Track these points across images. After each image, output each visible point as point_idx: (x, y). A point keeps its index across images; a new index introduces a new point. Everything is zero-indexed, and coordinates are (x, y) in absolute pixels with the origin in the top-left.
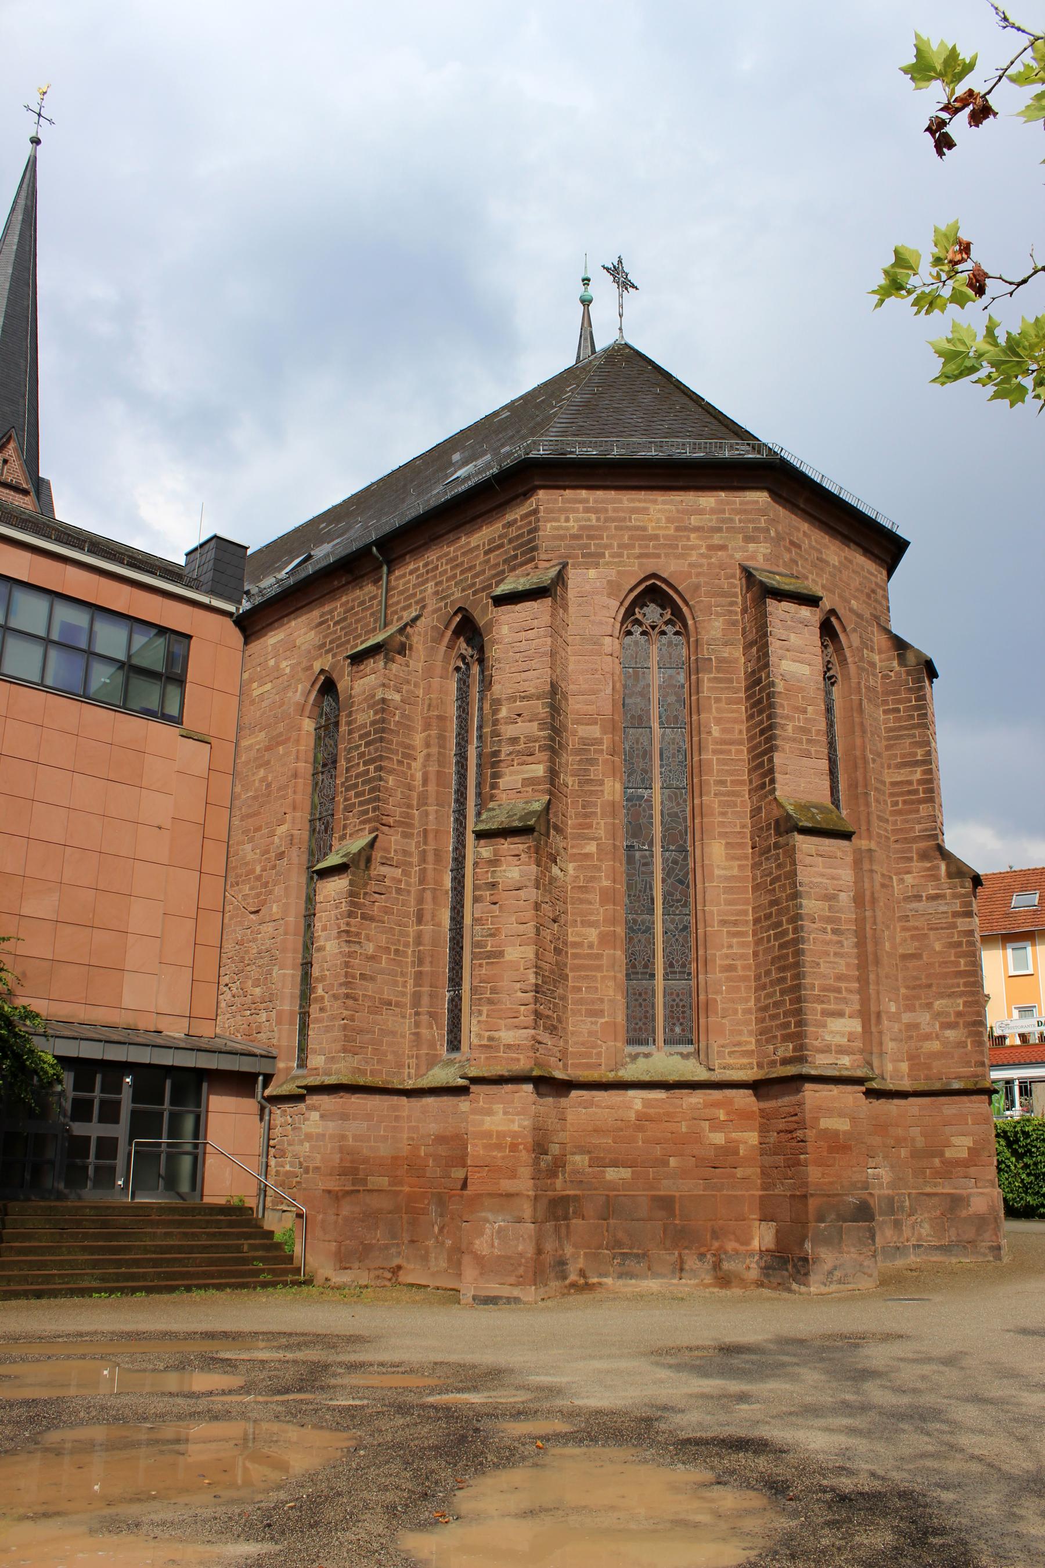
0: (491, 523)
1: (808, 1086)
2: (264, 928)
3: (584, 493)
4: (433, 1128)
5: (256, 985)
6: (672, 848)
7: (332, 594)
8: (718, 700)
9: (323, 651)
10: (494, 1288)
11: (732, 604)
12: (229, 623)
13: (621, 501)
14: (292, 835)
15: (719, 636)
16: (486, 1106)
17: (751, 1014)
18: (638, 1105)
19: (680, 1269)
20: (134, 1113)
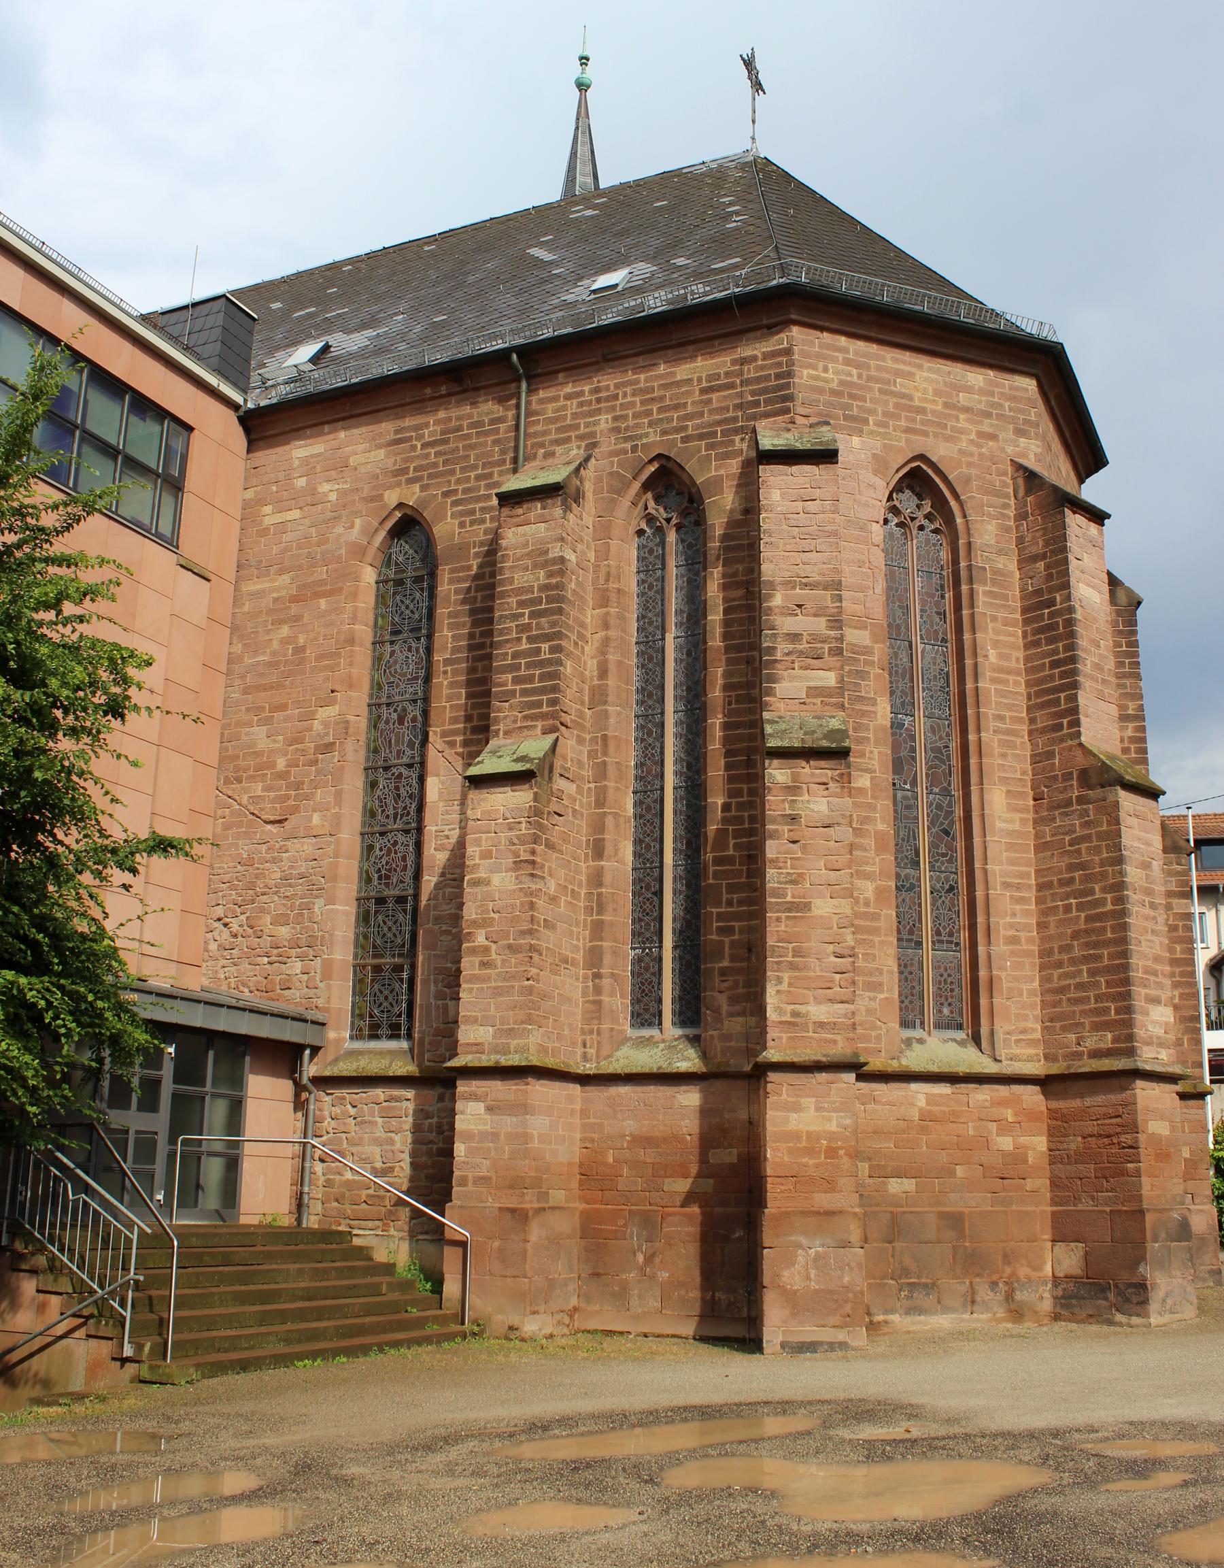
0: (711, 354)
1: (1139, 1083)
2: (294, 845)
3: (843, 341)
4: (630, 1126)
5: (281, 920)
6: (936, 790)
7: (419, 405)
8: (994, 619)
9: (403, 479)
10: (809, 1331)
11: (1006, 506)
12: (231, 417)
13: (884, 360)
14: (347, 722)
15: (993, 542)
16: (790, 1100)
17: (1036, 995)
18: (922, 1102)
19: (971, 1301)
20: (176, 1097)
